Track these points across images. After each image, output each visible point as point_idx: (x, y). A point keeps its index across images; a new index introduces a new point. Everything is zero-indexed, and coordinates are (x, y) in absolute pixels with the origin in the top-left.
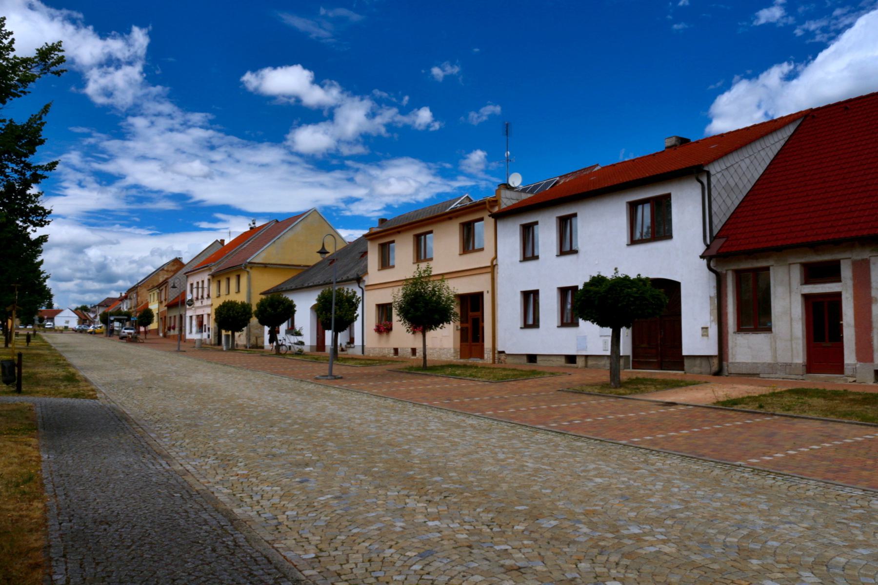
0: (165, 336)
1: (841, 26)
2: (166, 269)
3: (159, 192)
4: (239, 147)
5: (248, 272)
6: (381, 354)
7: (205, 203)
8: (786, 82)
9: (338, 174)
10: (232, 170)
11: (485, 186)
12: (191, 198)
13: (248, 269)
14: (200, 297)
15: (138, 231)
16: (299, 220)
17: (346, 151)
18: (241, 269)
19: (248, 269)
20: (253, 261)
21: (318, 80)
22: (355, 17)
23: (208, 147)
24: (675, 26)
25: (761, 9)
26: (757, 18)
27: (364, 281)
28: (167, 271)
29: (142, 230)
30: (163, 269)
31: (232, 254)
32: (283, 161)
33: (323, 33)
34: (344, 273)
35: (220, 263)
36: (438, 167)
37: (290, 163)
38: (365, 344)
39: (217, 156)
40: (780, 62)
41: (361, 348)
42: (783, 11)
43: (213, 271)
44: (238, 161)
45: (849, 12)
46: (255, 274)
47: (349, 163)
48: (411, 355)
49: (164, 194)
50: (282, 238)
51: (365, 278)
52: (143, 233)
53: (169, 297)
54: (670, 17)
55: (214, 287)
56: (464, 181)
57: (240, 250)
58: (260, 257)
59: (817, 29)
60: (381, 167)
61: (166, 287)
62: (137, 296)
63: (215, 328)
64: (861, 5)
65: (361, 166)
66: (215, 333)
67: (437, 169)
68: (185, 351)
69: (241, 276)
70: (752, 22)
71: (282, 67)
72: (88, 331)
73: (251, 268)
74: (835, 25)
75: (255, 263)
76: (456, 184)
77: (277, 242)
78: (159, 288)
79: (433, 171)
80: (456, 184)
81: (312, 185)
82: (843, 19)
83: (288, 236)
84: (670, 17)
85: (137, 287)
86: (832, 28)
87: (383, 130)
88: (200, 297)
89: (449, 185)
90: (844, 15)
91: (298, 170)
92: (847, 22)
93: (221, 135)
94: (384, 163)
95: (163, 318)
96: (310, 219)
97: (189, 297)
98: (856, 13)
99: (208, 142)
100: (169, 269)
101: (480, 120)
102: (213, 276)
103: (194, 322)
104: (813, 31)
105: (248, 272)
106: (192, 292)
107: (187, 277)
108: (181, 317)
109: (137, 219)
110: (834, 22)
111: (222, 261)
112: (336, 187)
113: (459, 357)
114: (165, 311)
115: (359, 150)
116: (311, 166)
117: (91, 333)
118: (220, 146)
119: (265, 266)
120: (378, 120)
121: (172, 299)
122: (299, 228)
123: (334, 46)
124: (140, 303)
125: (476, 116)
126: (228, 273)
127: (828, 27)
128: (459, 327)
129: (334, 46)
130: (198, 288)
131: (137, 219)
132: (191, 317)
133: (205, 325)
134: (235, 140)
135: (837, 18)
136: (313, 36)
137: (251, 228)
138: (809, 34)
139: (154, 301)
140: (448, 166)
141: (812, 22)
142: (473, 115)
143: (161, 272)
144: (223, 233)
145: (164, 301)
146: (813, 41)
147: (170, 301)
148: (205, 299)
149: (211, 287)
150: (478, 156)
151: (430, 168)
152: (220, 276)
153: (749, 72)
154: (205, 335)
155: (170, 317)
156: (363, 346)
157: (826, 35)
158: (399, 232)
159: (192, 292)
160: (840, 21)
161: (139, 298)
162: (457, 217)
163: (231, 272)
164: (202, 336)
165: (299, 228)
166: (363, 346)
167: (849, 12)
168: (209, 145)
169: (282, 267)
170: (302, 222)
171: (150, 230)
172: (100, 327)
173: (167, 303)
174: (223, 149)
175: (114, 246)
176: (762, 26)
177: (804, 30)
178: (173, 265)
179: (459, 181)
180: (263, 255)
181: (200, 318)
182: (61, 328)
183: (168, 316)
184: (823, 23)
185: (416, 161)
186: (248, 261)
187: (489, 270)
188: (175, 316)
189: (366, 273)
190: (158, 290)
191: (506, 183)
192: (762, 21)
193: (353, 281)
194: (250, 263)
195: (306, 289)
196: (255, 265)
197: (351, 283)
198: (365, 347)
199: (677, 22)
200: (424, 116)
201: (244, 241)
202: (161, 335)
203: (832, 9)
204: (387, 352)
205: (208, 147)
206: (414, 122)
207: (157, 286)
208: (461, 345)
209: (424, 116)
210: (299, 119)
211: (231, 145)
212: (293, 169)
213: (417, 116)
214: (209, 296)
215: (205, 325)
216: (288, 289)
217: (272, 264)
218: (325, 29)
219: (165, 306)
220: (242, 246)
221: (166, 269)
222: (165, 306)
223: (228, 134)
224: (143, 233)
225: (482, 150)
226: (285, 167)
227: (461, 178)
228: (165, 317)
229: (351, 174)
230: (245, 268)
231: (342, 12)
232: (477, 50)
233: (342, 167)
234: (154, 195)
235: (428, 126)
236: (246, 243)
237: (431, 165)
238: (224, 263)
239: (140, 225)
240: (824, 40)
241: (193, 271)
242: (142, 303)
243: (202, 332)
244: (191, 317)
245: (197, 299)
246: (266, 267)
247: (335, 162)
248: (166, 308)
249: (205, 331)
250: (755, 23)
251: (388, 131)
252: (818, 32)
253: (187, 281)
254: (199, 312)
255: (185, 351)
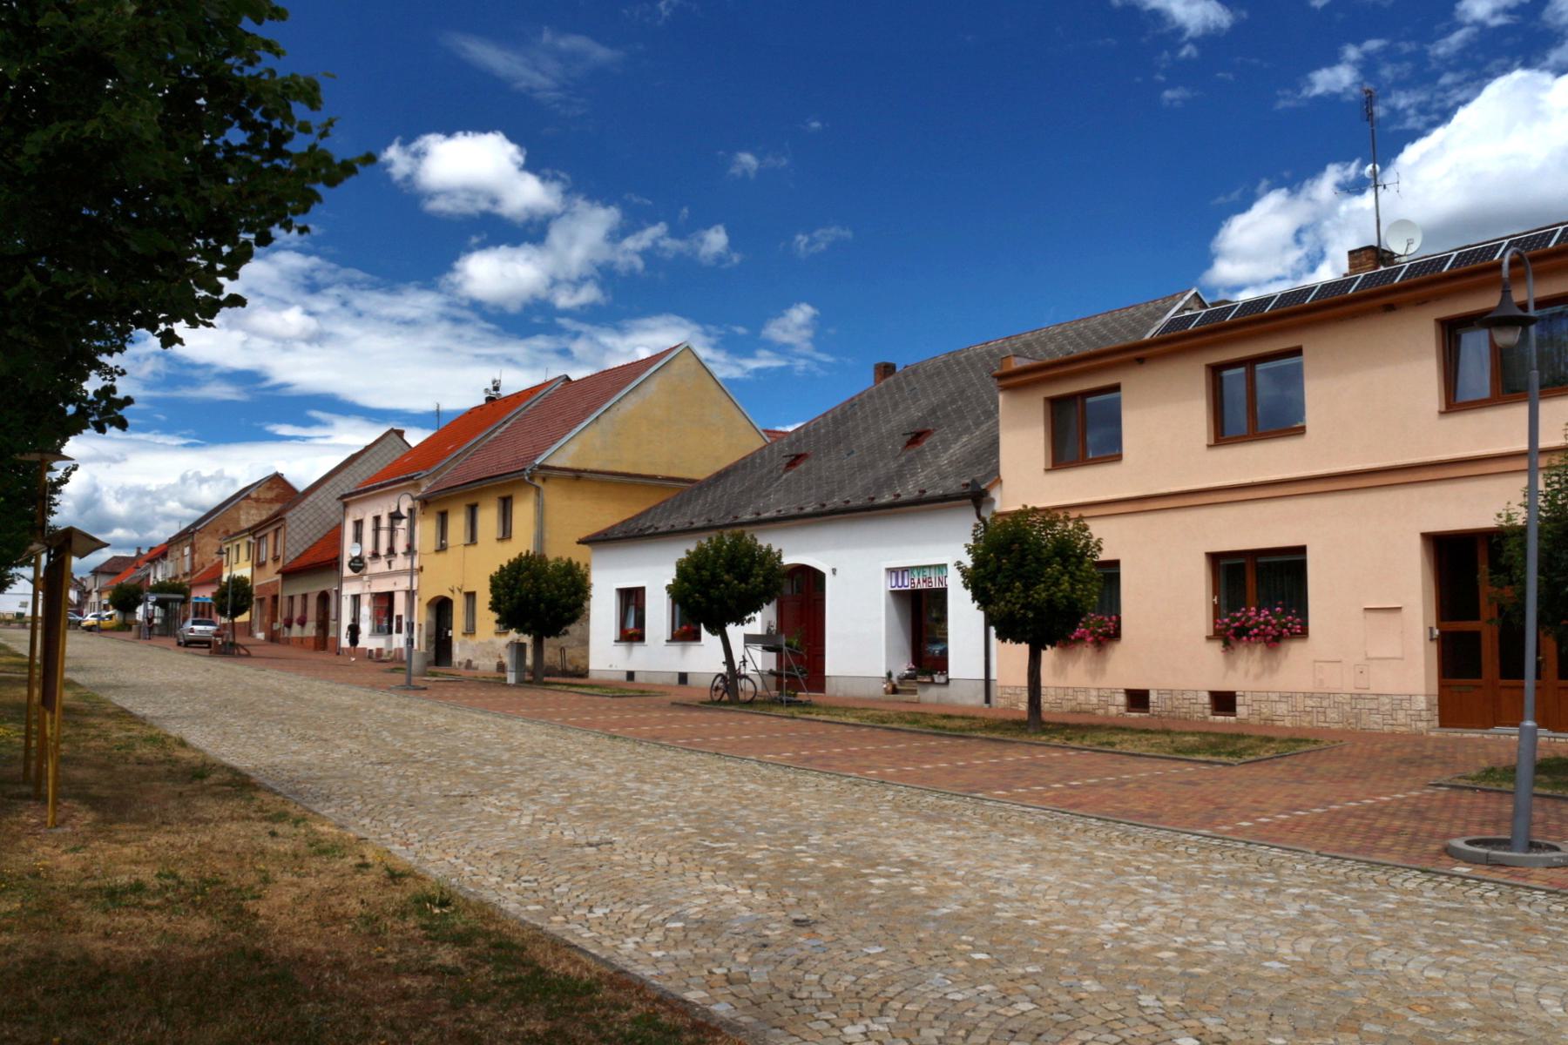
0: (273, 638)
1: (1450, 103)
2: (254, 495)
3: (207, 366)
4: (362, 289)
5: (538, 488)
6: (1067, 706)
7: (290, 389)
8: (1344, 194)
9: (540, 342)
10: (347, 329)
11: (802, 368)
12: (265, 379)
13: (538, 482)
14: (383, 550)
15: (162, 439)
16: (652, 370)
17: (564, 300)
18: (513, 484)
19: (538, 482)
20: (550, 463)
21: (533, 164)
22: (602, 54)
23: (306, 286)
24: (1168, 94)
25: (1318, 67)
26: (1312, 85)
27: (993, 501)
28: (257, 500)
29: (170, 437)
30: (248, 497)
31: (466, 451)
32: (443, 317)
33: (539, 80)
34: (888, 482)
35: (439, 472)
36: (723, 332)
37: (457, 321)
38: (994, 675)
39: (321, 304)
40: (1344, 158)
41: (982, 685)
42: (1355, 74)
43: (423, 489)
44: (359, 314)
45: (1467, 80)
46: (555, 497)
47: (565, 322)
48: (1208, 712)
49: (216, 370)
50: (614, 409)
51: (995, 494)
52: (169, 443)
53: (287, 553)
54: (1161, 78)
55: (426, 530)
56: (768, 358)
57: (485, 442)
58: (566, 453)
59: (1410, 106)
60: (621, 331)
61: (276, 531)
62: (193, 551)
63: (428, 624)
64: (1487, 69)
65: (585, 328)
66: (428, 636)
67: (719, 336)
68: (425, 689)
69: (514, 500)
70: (1299, 91)
71: (465, 134)
72: (84, 624)
73: (544, 480)
74: (1441, 100)
75: (554, 468)
76: (752, 364)
77: (603, 420)
78: (253, 535)
79: (713, 340)
80: (752, 364)
81: (491, 360)
82: (1454, 91)
83: (628, 405)
84: (1161, 78)
85: (193, 533)
86: (1436, 106)
87: (639, 264)
88: (383, 550)
89: (739, 366)
90: (1458, 85)
91: (468, 332)
92: (1461, 97)
93: (333, 266)
94: (626, 324)
95: (268, 601)
96: (676, 367)
97: (350, 550)
98: (1477, 83)
99: (307, 277)
100: (262, 496)
101: (813, 249)
102: (425, 502)
103: (366, 610)
104: (1404, 110)
105: (538, 488)
106: (358, 538)
107: (346, 505)
108: (324, 598)
109: (162, 417)
110: (1440, 95)
111: (445, 467)
112: (534, 365)
113: (1437, 723)
114: (277, 581)
115: (589, 294)
116: (492, 326)
117: (90, 629)
118: (328, 286)
119: (577, 477)
120: (630, 243)
121: (292, 557)
122: (653, 389)
123: (557, 106)
124: (198, 567)
125: (806, 239)
126: (473, 493)
127: (1430, 103)
128: (1436, 632)
129: (557, 106)
130: (377, 530)
131: (162, 417)
132: (356, 598)
133: (399, 617)
134: (359, 275)
135: (1445, 89)
136: (522, 85)
137: (490, 399)
138: (1396, 114)
139: (237, 562)
140: (741, 330)
141: (1402, 94)
142: (802, 239)
143: (243, 503)
144: (318, 445)
145: (270, 563)
146: (1401, 127)
147: (287, 561)
148: (400, 555)
149: (417, 528)
150: (801, 314)
151: (708, 334)
152: (448, 499)
153: (1286, 174)
154: (399, 641)
155: (291, 598)
156: (987, 680)
157: (1424, 119)
158: (1141, 361)
159: (358, 538)
160: (1450, 94)
161: (196, 556)
162: (1422, 302)
163: (483, 491)
164: (390, 642)
165: (652, 387)
166: (987, 680)
167: (1467, 80)
168: (308, 282)
169: (615, 478)
170: (660, 374)
171: (184, 436)
172: (110, 617)
173: (280, 566)
174: (333, 291)
175: (115, 467)
176: (1318, 98)
177: (1388, 108)
178: (270, 489)
179: (761, 359)
180: (573, 449)
181: (384, 601)
182: (9, 617)
183: (284, 595)
184: (1421, 97)
185: (685, 322)
186: (538, 462)
187: (1523, 464)
188: (305, 596)
189: (994, 475)
190: (251, 539)
191: (1376, 245)
192: (1319, 89)
193: (965, 501)
194: (541, 467)
195: (772, 526)
196: (556, 473)
197: (888, 514)
198: (993, 685)
199: (1171, 85)
200: (716, 240)
201: (492, 423)
202: (260, 636)
203: (1439, 75)
204: (1094, 700)
205: (306, 286)
206: (696, 253)
207: (249, 530)
208: (1442, 686)
209: (716, 240)
210: (485, 236)
211: (351, 284)
212: (461, 330)
213: (702, 241)
214: (410, 550)
215: (399, 617)
216: (678, 527)
217: (592, 472)
218: (544, 73)
219: (278, 572)
220: (489, 435)
221: (254, 495)
222: (278, 572)
223: (344, 263)
224: (169, 443)
225: (812, 304)
226: (445, 327)
227: (762, 353)
228: (275, 598)
229: (565, 342)
230: (531, 478)
231: (572, 42)
232: (816, 125)
233: (551, 329)
234: (197, 373)
235: (719, 259)
236: (500, 427)
237: (712, 328)
238: (451, 472)
239: (168, 429)
240: (1420, 126)
241: (366, 491)
242: (203, 566)
243: (390, 632)
244: (356, 598)
245: (376, 555)
246: (578, 478)
247: (537, 320)
248: (279, 577)
249: (399, 631)
250: (1305, 92)
251: (647, 267)
252: (1411, 112)
253: (344, 514)
254: (383, 586)
255: (425, 689)
